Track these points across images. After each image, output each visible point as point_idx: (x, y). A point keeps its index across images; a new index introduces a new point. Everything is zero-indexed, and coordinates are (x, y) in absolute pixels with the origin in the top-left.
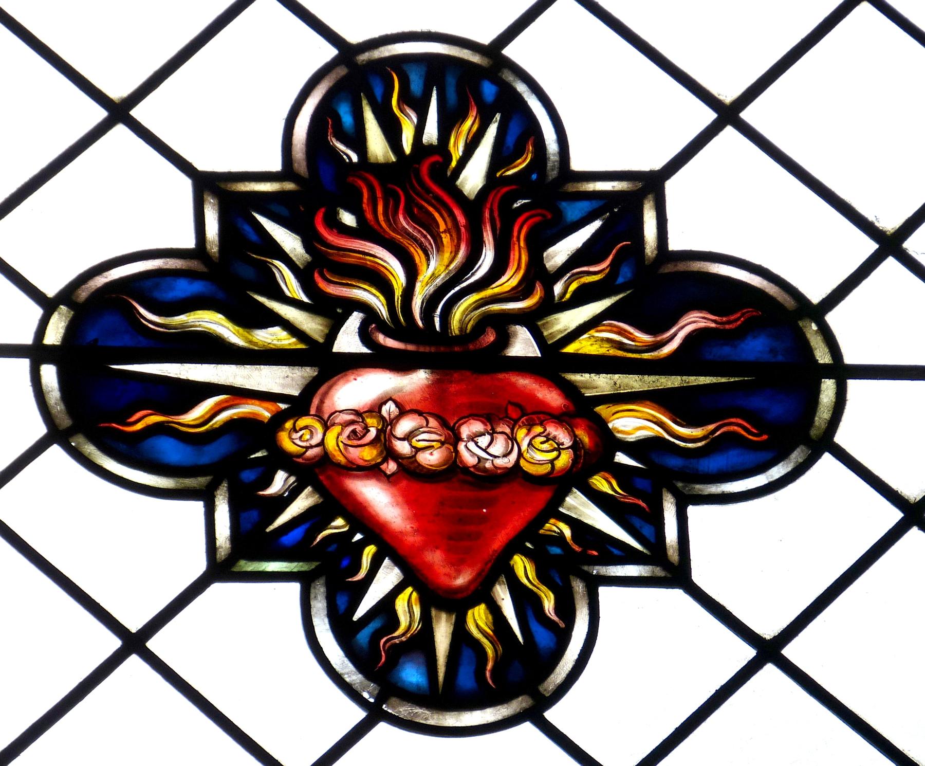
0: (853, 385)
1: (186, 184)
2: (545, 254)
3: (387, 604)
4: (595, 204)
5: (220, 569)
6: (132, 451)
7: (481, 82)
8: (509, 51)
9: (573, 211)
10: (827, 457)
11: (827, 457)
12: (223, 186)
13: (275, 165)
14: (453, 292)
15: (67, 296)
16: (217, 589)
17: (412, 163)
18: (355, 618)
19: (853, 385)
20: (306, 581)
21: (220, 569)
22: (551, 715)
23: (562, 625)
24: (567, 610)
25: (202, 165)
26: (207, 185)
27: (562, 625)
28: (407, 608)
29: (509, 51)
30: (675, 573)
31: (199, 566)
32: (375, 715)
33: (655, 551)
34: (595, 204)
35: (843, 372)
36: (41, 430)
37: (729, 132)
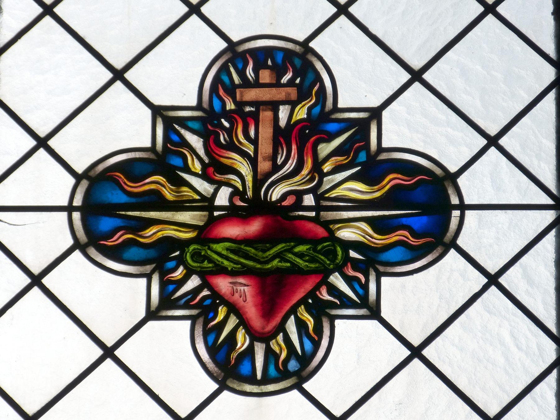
0: (468, 213)
1: (148, 112)
2: (318, 148)
3: (233, 334)
4: (342, 125)
5: (152, 314)
6: (114, 253)
7: (297, 64)
8: (312, 44)
9: (332, 127)
10: (452, 252)
11: (452, 252)
12: (164, 113)
13: (193, 102)
14: (305, 188)
15: (86, 174)
16: (151, 324)
17: (267, 83)
18: (241, 190)
19: (468, 213)
20: (193, 319)
21: (152, 314)
22: (223, 45)
23: (316, 338)
24: (319, 329)
25: (157, 101)
26: (158, 111)
27: (316, 338)
28: (242, 340)
29: (312, 44)
30: (374, 312)
31: (142, 314)
32: (223, 387)
33: (364, 301)
34: (342, 125)
35: (463, 207)
36: (462, 181)
37: (417, 85)
